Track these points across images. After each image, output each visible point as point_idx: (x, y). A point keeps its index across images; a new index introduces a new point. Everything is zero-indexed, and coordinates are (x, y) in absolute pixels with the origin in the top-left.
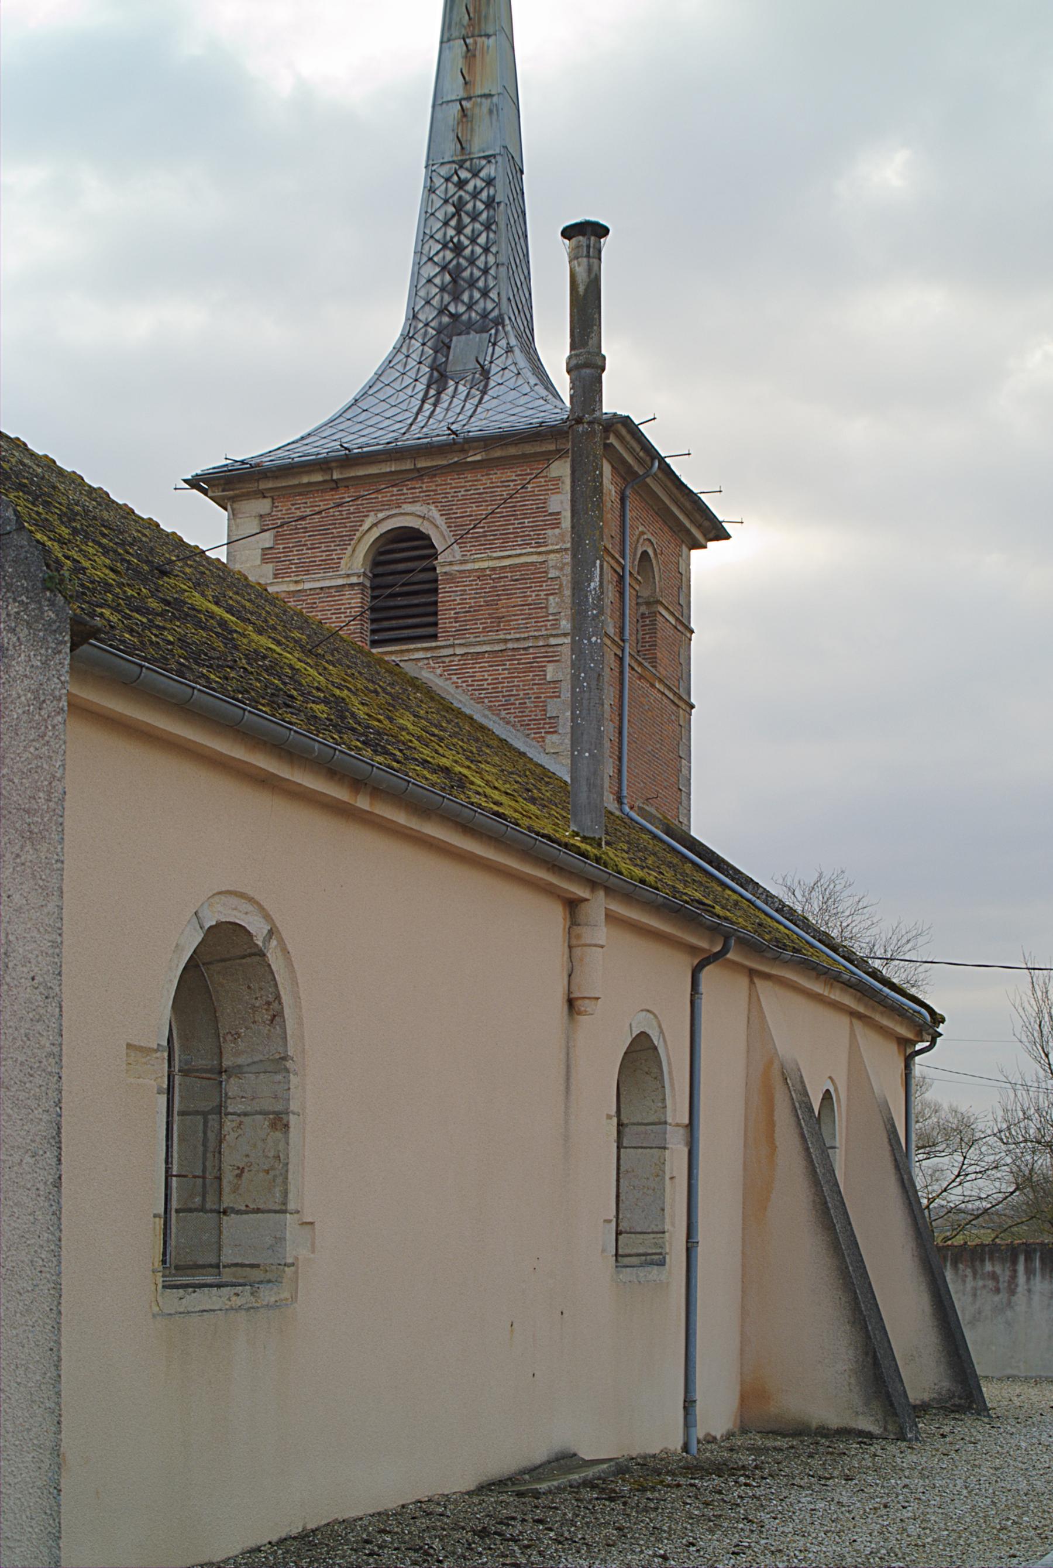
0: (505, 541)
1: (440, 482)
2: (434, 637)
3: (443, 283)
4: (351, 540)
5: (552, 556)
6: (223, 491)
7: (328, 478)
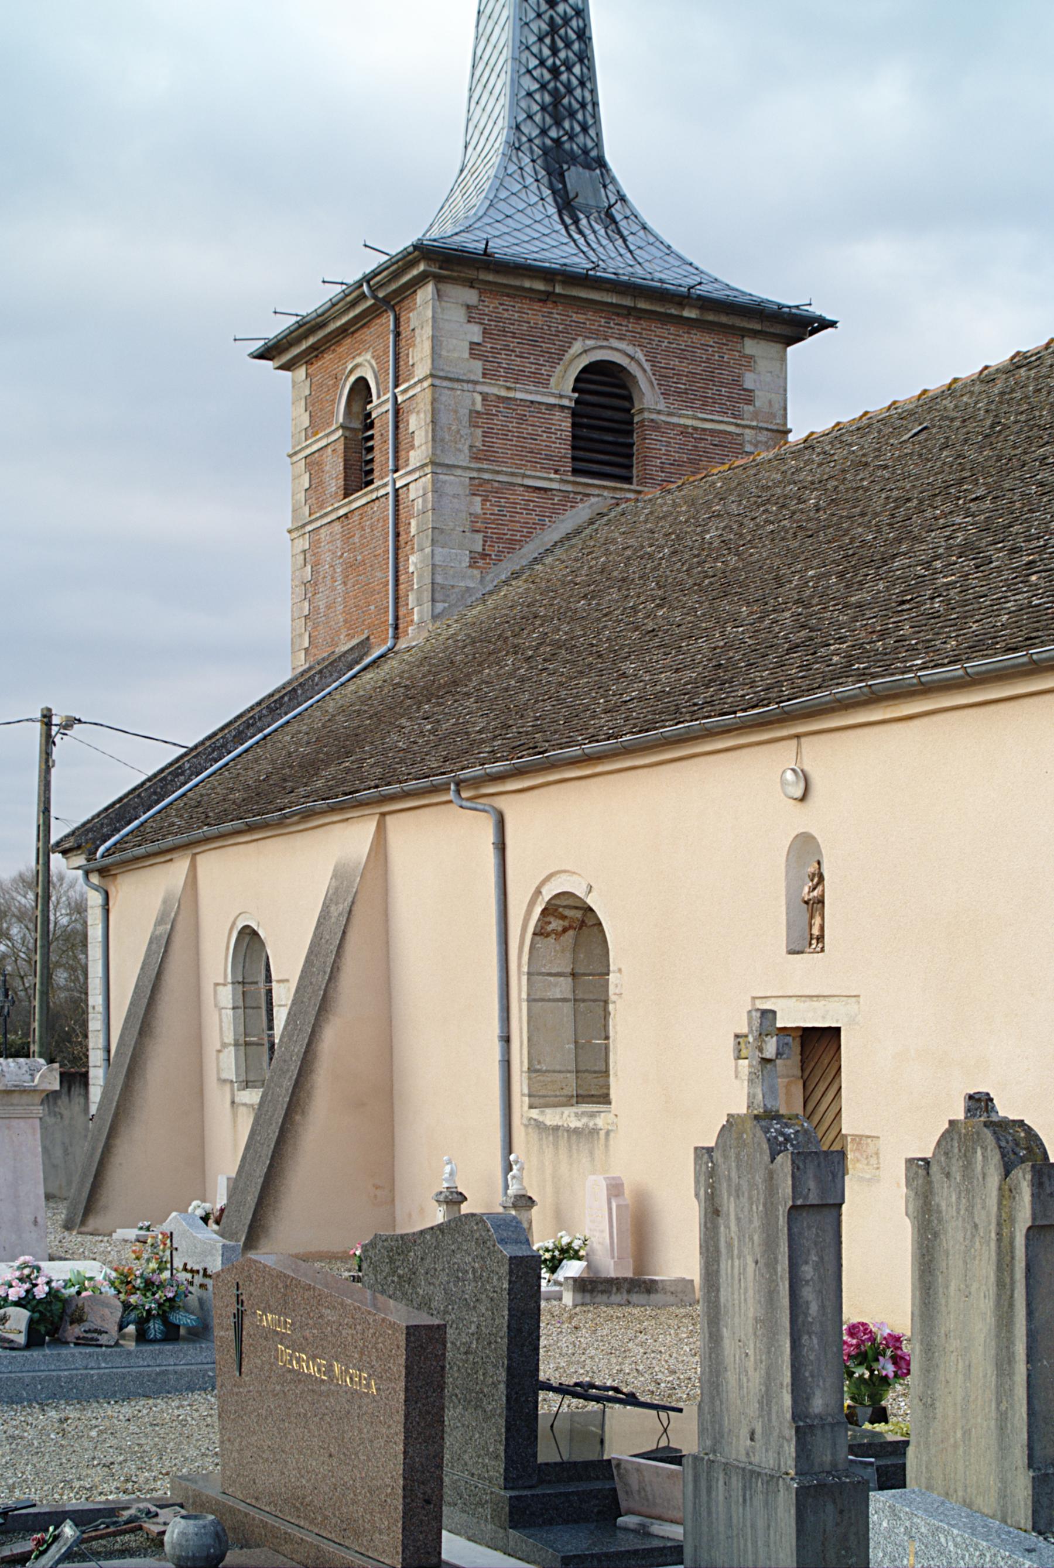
0: (705, 404)
1: (644, 326)
2: (628, 480)
3: (543, 101)
4: (561, 359)
5: (747, 431)
6: (440, 268)
7: (550, 289)
